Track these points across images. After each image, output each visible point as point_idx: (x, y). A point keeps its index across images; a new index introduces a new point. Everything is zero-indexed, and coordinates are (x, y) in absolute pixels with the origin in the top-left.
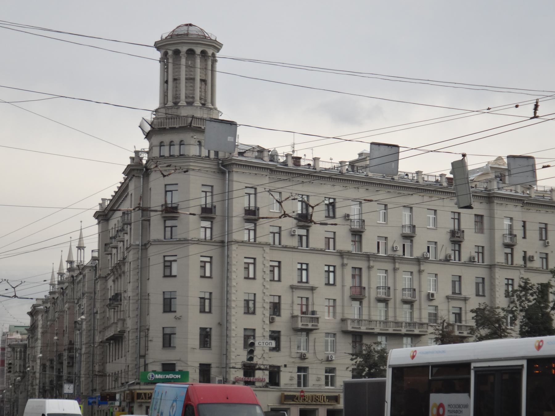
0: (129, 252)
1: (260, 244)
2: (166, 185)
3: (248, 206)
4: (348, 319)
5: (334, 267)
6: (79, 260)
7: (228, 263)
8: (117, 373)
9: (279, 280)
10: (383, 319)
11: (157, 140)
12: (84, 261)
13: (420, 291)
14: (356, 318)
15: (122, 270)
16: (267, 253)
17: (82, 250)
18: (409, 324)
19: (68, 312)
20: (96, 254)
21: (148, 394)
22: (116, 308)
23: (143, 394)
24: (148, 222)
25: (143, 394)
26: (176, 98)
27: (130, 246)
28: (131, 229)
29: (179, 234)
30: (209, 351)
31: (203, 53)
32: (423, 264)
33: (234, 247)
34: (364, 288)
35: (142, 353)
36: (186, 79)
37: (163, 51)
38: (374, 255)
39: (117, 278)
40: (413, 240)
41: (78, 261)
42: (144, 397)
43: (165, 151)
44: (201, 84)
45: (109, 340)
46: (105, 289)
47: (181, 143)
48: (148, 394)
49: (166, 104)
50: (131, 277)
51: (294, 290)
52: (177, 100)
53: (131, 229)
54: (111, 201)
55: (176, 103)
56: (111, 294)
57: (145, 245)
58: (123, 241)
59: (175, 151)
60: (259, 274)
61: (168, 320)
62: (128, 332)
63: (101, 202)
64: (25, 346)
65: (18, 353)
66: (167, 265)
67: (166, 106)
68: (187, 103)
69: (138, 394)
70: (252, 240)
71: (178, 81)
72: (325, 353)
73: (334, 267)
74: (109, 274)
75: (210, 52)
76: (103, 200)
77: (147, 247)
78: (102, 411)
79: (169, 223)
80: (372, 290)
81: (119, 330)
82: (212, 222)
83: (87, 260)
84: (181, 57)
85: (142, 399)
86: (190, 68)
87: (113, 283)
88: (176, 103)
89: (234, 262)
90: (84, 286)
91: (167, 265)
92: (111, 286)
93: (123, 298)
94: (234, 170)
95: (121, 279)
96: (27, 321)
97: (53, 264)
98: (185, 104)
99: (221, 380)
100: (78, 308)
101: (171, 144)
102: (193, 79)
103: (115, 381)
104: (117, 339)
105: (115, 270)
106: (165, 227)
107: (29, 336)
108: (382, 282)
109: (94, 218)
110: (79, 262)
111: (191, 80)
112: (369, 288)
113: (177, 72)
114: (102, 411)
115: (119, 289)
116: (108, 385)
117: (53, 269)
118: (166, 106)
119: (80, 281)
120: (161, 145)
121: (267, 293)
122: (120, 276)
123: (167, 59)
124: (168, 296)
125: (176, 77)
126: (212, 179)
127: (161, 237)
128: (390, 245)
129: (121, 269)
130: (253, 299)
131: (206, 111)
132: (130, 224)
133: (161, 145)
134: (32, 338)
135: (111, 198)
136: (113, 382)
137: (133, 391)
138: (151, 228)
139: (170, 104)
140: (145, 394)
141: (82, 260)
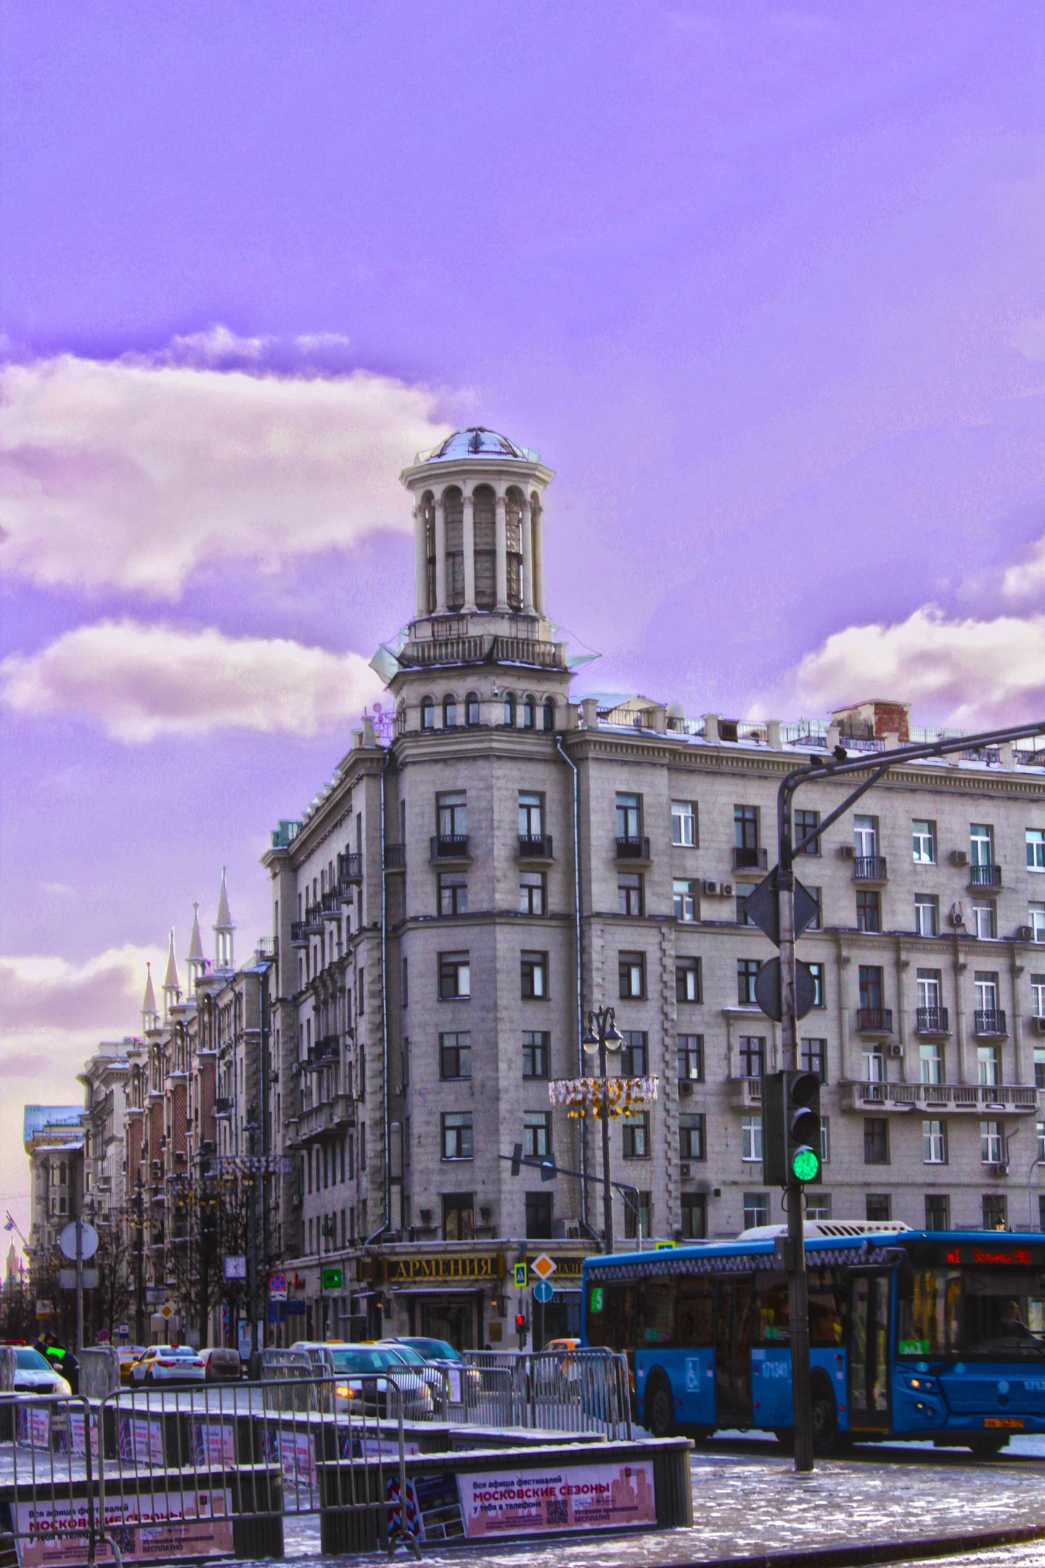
0: (359, 944)
1: (653, 918)
2: (439, 795)
3: (623, 835)
4: (854, 1082)
5: (820, 966)
6: (221, 957)
7: (582, 964)
8: (331, 1215)
9: (698, 999)
10: (933, 1080)
11: (413, 693)
12: (232, 960)
13: (1014, 1016)
14: (872, 1080)
15: (339, 985)
16: (669, 940)
17: (228, 937)
18: (995, 1091)
19: (199, 1078)
20: (269, 949)
21: (414, 1264)
22: (325, 1070)
23: (402, 1265)
24: (399, 879)
25: (402, 1265)
26: (456, 594)
27: (360, 934)
28: (360, 893)
29: (475, 900)
30: (893, 1197)
31: (513, 493)
32: (1020, 954)
33: (596, 928)
34: (889, 1012)
35: (396, 1171)
36: (477, 553)
37: (420, 493)
38: (908, 934)
39: (325, 1003)
40: (995, 901)
41: (218, 960)
42: (403, 1271)
43: (436, 718)
44: (509, 564)
45: (308, 1143)
46: (293, 1030)
47: (471, 699)
48: (414, 1264)
49: (433, 611)
50: (366, 1001)
51: (731, 1021)
52: (459, 602)
53: (360, 893)
54: (302, 827)
55: (455, 607)
56: (309, 1040)
57: (396, 928)
58: (339, 920)
59: (458, 715)
60: (653, 988)
61: (451, 1096)
62: (360, 1126)
63: (278, 828)
64: (77, 1155)
65: (57, 1172)
66: (447, 971)
67: (433, 615)
68: (479, 606)
69: (390, 1263)
70: (635, 911)
71: (458, 559)
72: (744, 1162)
73: (820, 966)
74: (302, 993)
75: (529, 489)
76: (284, 825)
77: (400, 933)
78: (340, 1302)
79: (448, 879)
80: (905, 1016)
81: (337, 1120)
82: (544, 875)
83: (244, 960)
84: (462, 505)
85: (401, 1275)
86: (485, 527)
87: (313, 1013)
88: (455, 607)
89: (596, 964)
90: (238, 1017)
91: (447, 971)
92: (309, 1021)
93: (341, 1048)
94: (591, 755)
95: (335, 1004)
96: (75, 1097)
97: (149, 964)
98: (475, 609)
99: (576, 1228)
100: (223, 1068)
101: (448, 701)
102: (492, 553)
103: (326, 1234)
104: (334, 1139)
105: (318, 983)
106: (440, 889)
107: (88, 1131)
108: (929, 997)
109: (262, 866)
110: (221, 962)
111: (486, 554)
112: (900, 1012)
113: (454, 538)
114: (340, 1302)
115: (331, 1027)
116: (307, 1243)
117: (149, 978)
118: (433, 615)
119: (227, 1007)
120: (426, 703)
121: (670, 1032)
122: (333, 997)
123: (432, 511)
124: (450, 1042)
125: (451, 550)
126: (542, 777)
127: (433, 911)
128: (944, 910)
129: (334, 981)
130: (641, 1044)
131: (522, 626)
132: (359, 883)
133: (426, 703)
134: (95, 1136)
135: (304, 821)
136: (323, 1239)
137: (380, 1258)
138: (408, 891)
139: (441, 610)
140: (406, 1264)
141: (228, 957)
